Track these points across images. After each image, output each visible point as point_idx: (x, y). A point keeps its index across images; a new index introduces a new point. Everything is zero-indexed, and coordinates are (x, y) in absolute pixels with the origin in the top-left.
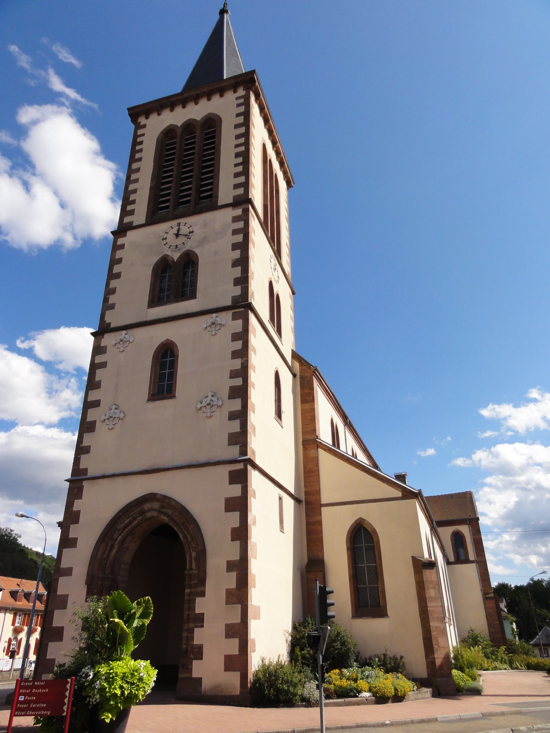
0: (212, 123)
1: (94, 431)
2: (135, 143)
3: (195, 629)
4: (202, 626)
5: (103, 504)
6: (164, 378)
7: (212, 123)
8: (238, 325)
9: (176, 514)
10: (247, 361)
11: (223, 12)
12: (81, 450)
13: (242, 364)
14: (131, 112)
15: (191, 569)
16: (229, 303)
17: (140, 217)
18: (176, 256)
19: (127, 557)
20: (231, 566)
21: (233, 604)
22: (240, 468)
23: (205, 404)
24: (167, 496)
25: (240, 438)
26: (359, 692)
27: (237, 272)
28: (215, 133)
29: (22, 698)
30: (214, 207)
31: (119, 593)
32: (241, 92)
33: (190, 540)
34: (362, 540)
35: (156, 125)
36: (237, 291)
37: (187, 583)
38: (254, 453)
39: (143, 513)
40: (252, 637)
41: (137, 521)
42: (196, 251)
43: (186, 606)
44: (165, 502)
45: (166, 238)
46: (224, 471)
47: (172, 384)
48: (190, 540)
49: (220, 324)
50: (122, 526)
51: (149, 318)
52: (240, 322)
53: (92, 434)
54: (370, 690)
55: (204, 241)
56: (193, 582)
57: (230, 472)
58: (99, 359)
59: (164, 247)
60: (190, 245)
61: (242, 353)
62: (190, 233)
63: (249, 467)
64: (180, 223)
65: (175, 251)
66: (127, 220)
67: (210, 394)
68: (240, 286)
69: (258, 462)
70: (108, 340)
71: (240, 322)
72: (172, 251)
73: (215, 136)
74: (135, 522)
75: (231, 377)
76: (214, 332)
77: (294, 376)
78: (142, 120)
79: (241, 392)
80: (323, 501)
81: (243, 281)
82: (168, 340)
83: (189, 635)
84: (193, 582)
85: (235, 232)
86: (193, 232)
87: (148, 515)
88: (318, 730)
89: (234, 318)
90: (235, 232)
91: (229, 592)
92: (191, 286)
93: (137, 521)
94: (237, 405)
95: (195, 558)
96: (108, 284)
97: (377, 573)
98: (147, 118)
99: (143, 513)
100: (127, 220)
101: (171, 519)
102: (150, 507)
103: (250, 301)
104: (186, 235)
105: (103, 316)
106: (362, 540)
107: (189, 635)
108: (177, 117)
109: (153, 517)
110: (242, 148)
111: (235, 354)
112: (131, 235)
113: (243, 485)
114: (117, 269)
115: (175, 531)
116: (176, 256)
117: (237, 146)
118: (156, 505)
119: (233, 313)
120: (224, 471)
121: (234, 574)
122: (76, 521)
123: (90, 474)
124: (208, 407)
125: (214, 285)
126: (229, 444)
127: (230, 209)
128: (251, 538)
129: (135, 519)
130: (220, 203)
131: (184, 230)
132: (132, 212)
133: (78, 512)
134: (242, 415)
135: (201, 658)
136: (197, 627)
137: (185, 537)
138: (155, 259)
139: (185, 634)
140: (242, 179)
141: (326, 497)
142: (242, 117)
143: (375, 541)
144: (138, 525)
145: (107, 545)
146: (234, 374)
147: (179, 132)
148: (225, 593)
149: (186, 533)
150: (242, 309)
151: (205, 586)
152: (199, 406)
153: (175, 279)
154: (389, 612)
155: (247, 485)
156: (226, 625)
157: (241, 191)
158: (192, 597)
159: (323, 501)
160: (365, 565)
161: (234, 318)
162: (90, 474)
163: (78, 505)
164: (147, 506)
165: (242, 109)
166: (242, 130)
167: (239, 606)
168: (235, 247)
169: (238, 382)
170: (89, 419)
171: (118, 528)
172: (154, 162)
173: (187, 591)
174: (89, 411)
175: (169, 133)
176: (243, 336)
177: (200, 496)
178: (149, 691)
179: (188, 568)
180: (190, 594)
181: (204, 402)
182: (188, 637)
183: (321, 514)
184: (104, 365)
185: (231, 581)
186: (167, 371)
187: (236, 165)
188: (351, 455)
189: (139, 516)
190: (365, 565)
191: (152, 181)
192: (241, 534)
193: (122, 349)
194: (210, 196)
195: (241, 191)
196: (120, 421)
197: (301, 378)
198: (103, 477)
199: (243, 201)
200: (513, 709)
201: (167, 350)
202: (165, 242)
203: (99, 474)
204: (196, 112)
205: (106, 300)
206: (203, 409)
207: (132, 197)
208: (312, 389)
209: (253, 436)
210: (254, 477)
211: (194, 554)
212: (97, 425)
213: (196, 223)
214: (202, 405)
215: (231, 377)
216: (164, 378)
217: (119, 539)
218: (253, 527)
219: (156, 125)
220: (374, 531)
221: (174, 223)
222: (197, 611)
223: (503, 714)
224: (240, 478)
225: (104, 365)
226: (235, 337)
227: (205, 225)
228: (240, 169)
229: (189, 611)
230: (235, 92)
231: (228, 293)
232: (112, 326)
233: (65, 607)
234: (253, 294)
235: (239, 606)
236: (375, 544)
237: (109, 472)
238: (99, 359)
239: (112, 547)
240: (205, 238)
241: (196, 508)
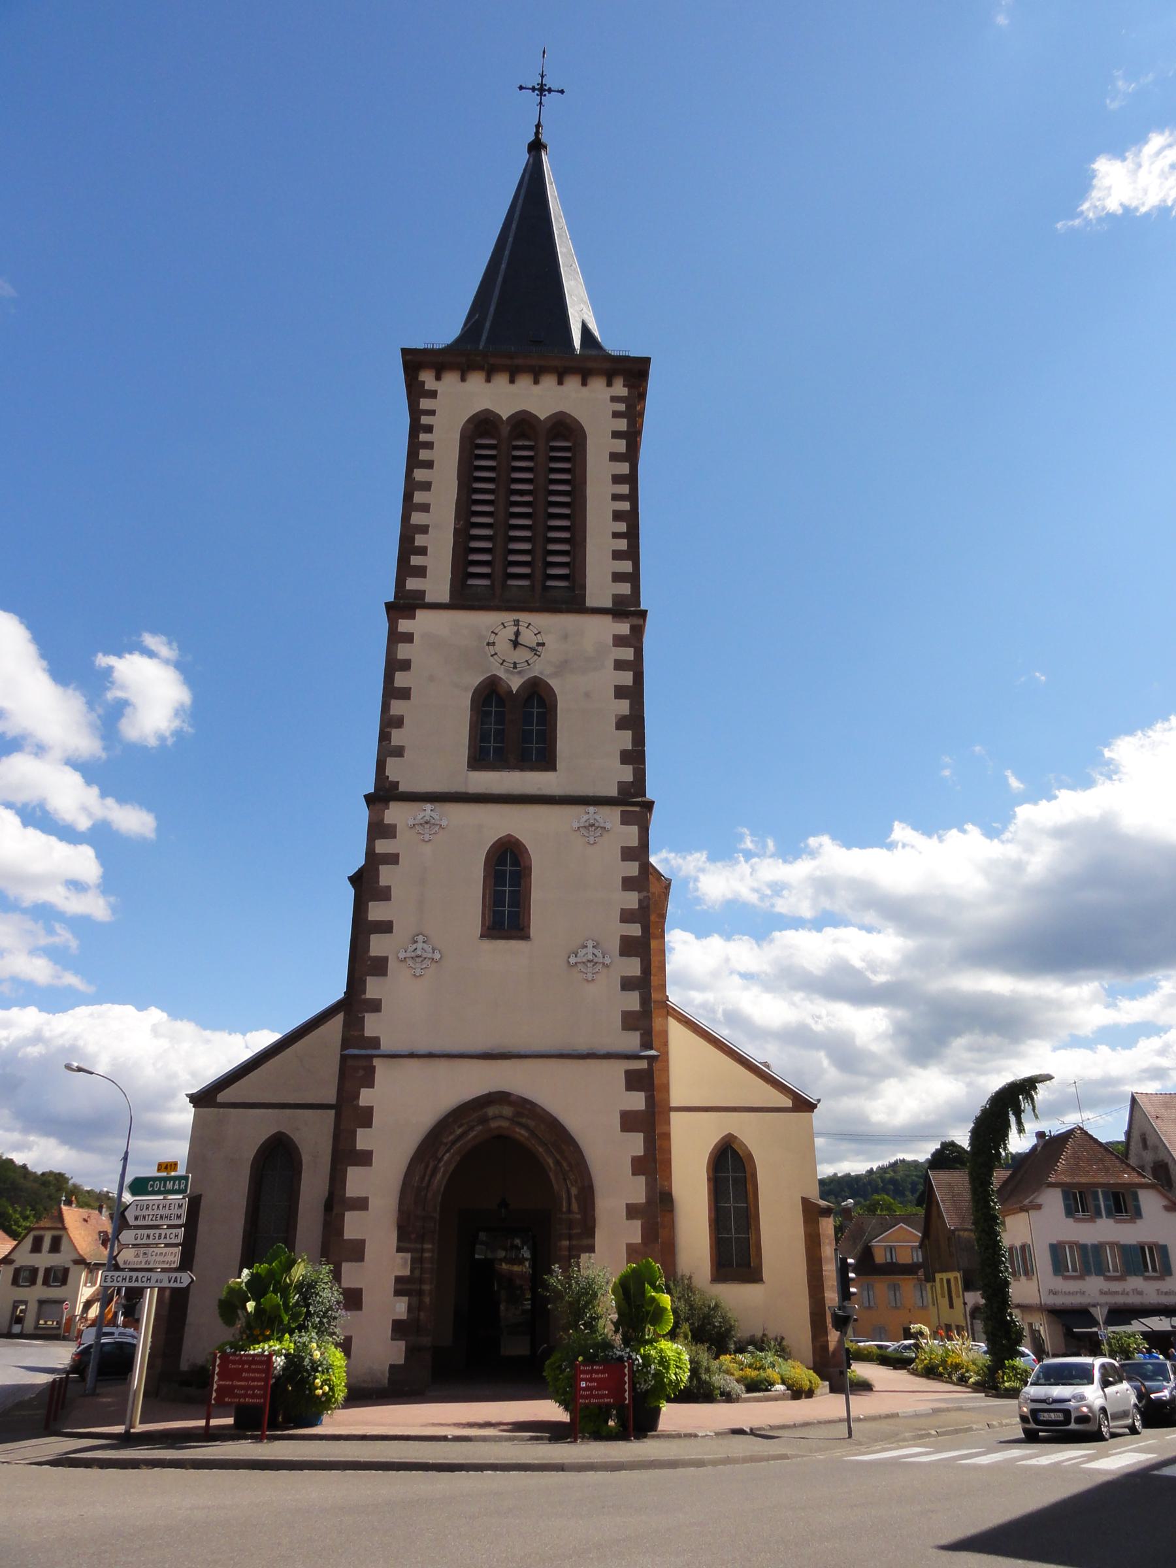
2: (416, 428)
6: (507, 900)
11: (536, 147)
15: (570, 1211)
26: (772, 1384)
27: (625, 739)
29: (583, 1384)
31: (648, 1262)
34: (730, 1167)
36: (627, 774)
42: (552, 682)
44: (525, 1108)
45: (494, 644)
50: (451, 1138)
51: (472, 789)
53: (381, 979)
54: (783, 1383)
55: (563, 667)
60: (540, 668)
62: (539, 644)
65: (512, 673)
70: (395, 814)
71: (634, 830)
72: (507, 671)
75: (623, 921)
76: (592, 840)
80: (673, 1104)
86: (543, 644)
87: (494, 1124)
88: (841, 1420)
90: (620, 665)
96: (385, 707)
97: (747, 1217)
99: (484, 1120)
101: (532, 1132)
102: (497, 1112)
104: (532, 649)
106: (730, 1167)
114: (401, 679)
118: (507, 1111)
124: (589, 965)
125: (586, 751)
127: (607, 620)
129: (471, 1128)
131: (527, 637)
137: (558, 1163)
141: (677, 1097)
143: (747, 1168)
145: (427, 1167)
149: (558, 1157)
150: (637, 809)
152: (573, 960)
153: (514, 726)
154: (766, 1273)
159: (673, 1104)
160: (731, 1204)
164: (491, 1111)
171: (445, 1141)
172: (458, 479)
183: (669, 1123)
190: (731, 1204)
193: (427, 837)
196: (434, 965)
198: (412, 1056)
202: (492, 650)
203: (403, 1048)
205: (384, 737)
206: (580, 966)
207: (420, 540)
211: (574, 1191)
215: (623, 921)
216: (507, 900)
217: (445, 1158)
220: (750, 1156)
221: (508, 617)
223: (948, 1410)
227: (565, 637)
232: (402, 788)
233: (360, 1258)
236: (748, 1175)
237: (423, 1049)
239: (435, 1170)
240: (566, 661)
241: (573, 1121)
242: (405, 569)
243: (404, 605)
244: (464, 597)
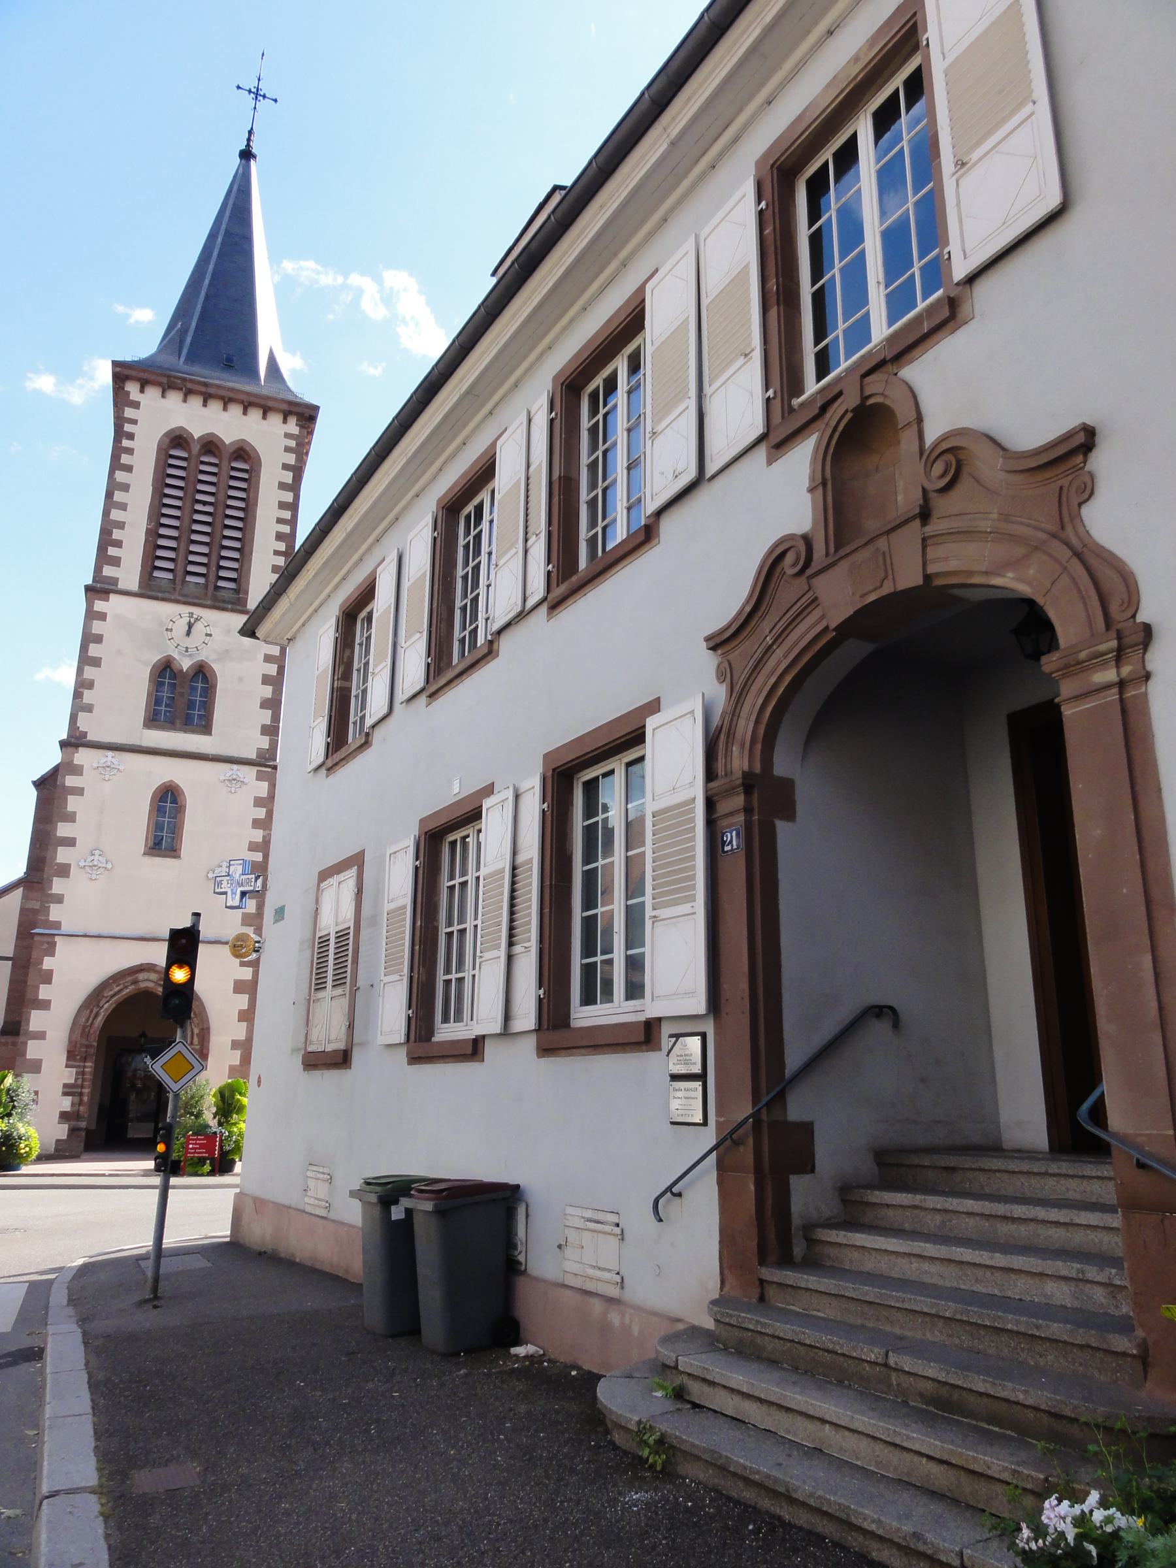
14: (118, 369)
16: (253, 755)
18: (186, 664)
20: (235, 1045)
36: (264, 742)
42: (214, 666)
72: (180, 653)
87: (143, 985)
89: (259, 778)
99: (135, 982)
105: (73, 719)
116: (186, 664)
121: (238, 1053)
123: (65, 929)
129: (126, 987)
133: (51, 972)
135: (50, 983)
161: (259, 778)
162: (65, 929)
164: (141, 976)
168: (266, 680)
178: (311, 264)
200: (949, 1309)
202: (169, 634)
211: (196, 1031)
231: (252, 743)
239: (97, 1014)
242: (103, 559)
243: (99, 589)
244: (149, 589)
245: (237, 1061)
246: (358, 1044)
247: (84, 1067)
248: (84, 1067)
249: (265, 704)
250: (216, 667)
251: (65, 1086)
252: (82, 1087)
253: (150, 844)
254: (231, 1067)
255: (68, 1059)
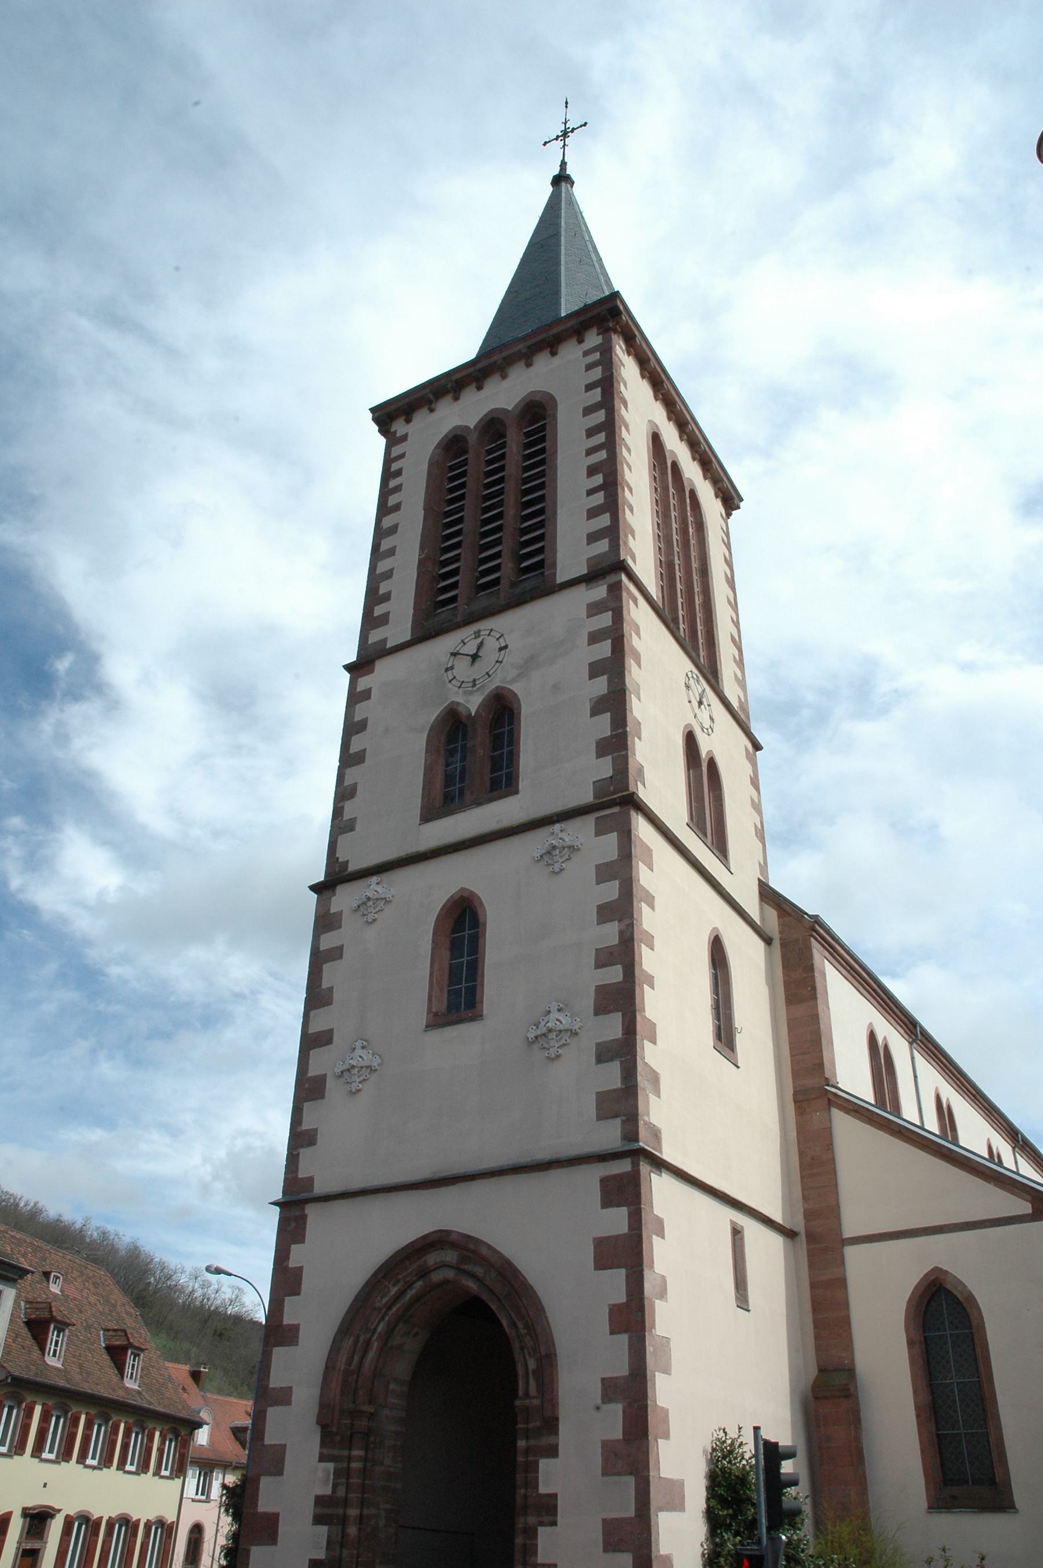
0: (537, 414)
1: (322, 1097)
3: (541, 1529)
4: (554, 1523)
5: (354, 1248)
7: (537, 414)
8: (609, 845)
9: (493, 1274)
10: (632, 925)
12: (301, 1138)
13: (621, 933)
15: (527, 1394)
16: (587, 797)
17: (400, 629)
18: (473, 703)
19: (402, 1368)
20: (611, 1389)
21: (618, 1474)
22: (626, 1167)
23: (544, 1030)
24: (505, 797)
25: (623, 1102)
28: (544, 430)
30: (549, 589)
32: (593, 339)
33: (523, 1332)
35: (429, 431)
37: (520, 1426)
38: (656, 1134)
39: (424, 1273)
40: (663, 1551)
41: (414, 1291)
43: (520, 1477)
46: (588, 1181)
47: (474, 987)
48: (523, 1332)
49: (569, 847)
50: (385, 1300)
51: (423, 846)
52: (612, 839)
56: (531, 1425)
57: (603, 1181)
58: (328, 941)
59: (450, 686)
61: (621, 909)
63: (644, 1168)
64: (479, 631)
65: (471, 692)
66: (375, 636)
67: (554, 1007)
68: (610, 757)
69: (668, 1154)
71: (612, 839)
72: (465, 693)
73: (544, 436)
74: (411, 1293)
75: (600, 964)
77: (768, 941)
78: (399, 427)
79: (621, 998)
81: (617, 744)
82: (463, 889)
83: (528, 1542)
84: (531, 1425)
85: (594, 638)
87: (437, 1277)
91: (608, 1447)
92: (508, 746)
93: (414, 1291)
94: (612, 1027)
95: (534, 1372)
98: (408, 421)
99: (424, 1273)
100: (375, 636)
103: (632, 789)
107: (528, 1542)
108: (466, 413)
109: (446, 1282)
110: (603, 455)
111: (606, 913)
112: (385, 670)
113: (633, 1207)
115: (493, 1313)
116: (473, 703)
117: (589, 452)
118: (450, 1256)
119: (597, 819)
120: (588, 1181)
121: (617, 1410)
122: (296, 1290)
123: (319, 1189)
125: (553, 766)
126: (599, 1118)
127: (582, 588)
128: (653, 1326)
129: (410, 1286)
130: (560, 579)
132: (384, 620)
134: (624, 1051)
136: (542, 1524)
138: (433, 714)
139: (519, 1540)
140: (604, 520)
142: (598, 390)
144: (417, 1298)
146: (604, 959)
147: (472, 440)
148: (599, 1450)
150: (616, 810)
151: (557, 1433)
155: (640, 1209)
156: (604, 1520)
157: (602, 546)
158: (531, 1458)
163: (298, 1255)
164: (432, 1259)
165: (597, 373)
166: (600, 416)
167: (631, 1480)
168: (595, 670)
169: (614, 974)
170: (313, 1072)
171: (377, 1305)
173: (521, 1444)
174: (313, 1053)
175: (454, 444)
176: (620, 870)
177: (541, 1237)
179: (520, 1393)
180: (527, 1451)
181: (543, 1023)
182: (524, 1545)
184: (336, 953)
185: (612, 1423)
186: (465, 959)
187: (590, 492)
188: (987, 1156)
189: (418, 1280)
191: (422, 548)
192: (631, 1318)
194: (541, 565)
195: (602, 546)
197: (784, 945)
199: (610, 569)
201: (465, 910)
204: (505, 394)
208: (810, 968)
209: (652, 1097)
210: (662, 1193)
211: (532, 1364)
212: (330, 1083)
213: (516, 628)
214: (539, 1032)
215: (600, 964)
217: (379, 1329)
218: (657, 1302)
219: (429, 431)
222: (543, 1490)
224: (626, 1194)
225: (336, 953)
226: (604, 873)
228: (599, 498)
229: (526, 1488)
230: (581, 341)
231: (580, 777)
234: (640, 771)
235: (631, 1480)
238: (328, 941)
239: (368, 1344)
240: (532, 657)
245: (617, 1433)
246: (787, 410)
247: (350, 1459)
248: (350, 1459)
249: (598, 707)
250: (517, 688)
251: (320, 1501)
252: (345, 1503)
253: (442, 1005)
254: (606, 1445)
255: (323, 1444)
